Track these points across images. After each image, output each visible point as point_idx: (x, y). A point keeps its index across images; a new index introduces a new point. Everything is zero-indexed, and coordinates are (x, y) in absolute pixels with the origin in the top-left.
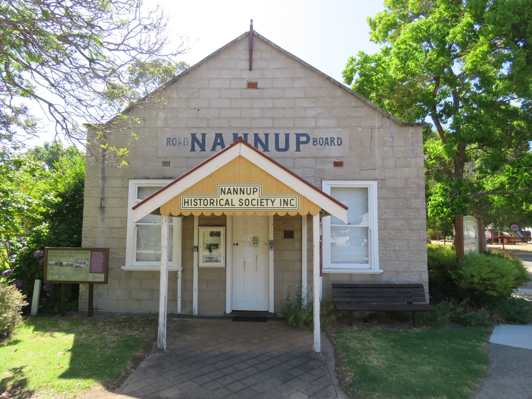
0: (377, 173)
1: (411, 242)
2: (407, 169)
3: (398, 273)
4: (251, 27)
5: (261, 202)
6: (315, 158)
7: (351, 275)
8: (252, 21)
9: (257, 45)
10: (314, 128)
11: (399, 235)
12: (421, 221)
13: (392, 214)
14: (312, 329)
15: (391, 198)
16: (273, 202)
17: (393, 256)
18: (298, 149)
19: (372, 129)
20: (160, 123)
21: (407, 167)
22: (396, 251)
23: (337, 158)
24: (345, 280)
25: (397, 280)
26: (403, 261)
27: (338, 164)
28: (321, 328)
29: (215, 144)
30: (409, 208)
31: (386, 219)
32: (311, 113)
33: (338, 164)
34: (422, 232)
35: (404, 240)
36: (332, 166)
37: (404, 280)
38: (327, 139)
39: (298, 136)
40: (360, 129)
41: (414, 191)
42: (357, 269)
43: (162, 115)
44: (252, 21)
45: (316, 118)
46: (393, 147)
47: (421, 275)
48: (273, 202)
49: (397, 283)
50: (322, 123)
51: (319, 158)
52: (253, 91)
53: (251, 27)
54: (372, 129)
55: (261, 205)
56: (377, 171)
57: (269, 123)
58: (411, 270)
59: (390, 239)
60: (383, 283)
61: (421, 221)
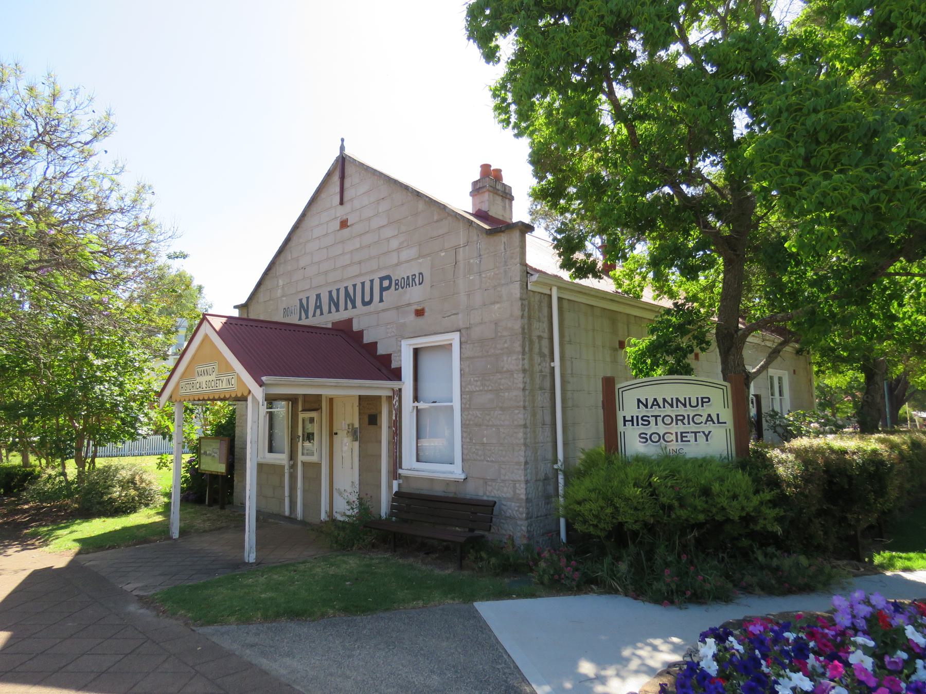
0: (460, 320)
1: (501, 430)
2: (497, 306)
3: (485, 482)
4: (342, 148)
5: (682, 437)
6: (397, 308)
7: (431, 480)
8: (343, 140)
9: (349, 170)
10: (397, 265)
11: (488, 418)
12: (515, 393)
13: (479, 383)
14: (259, 512)
15: (478, 357)
16: (707, 436)
17: (480, 452)
18: (381, 300)
19: (456, 249)
20: (279, 292)
21: (498, 303)
22: (483, 444)
23: (419, 303)
24: (425, 489)
25: (485, 494)
26: (492, 461)
27: (420, 313)
28: (533, 595)
29: (316, 307)
30: (500, 372)
31: (471, 393)
32: (394, 244)
33: (420, 313)
34: (516, 411)
35: (493, 426)
36: (412, 317)
37: (493, 494)
38: (408, 277)
39: (702, 398)
40: (443, 254)
41: (505, 342)
42: (444, 473)
43: (281, 283)
44: (343, 140)
45: (399, 250)
46: (480, 273)
47: (515, 487)
48: (707, 436)
49: (485, 498)
50: (405, 255)
51: (401, 307)
52: (346, 231)
53: (342, 148)
54: (456, 249)
55: (682, 441)
56: (460, 316)
57: (355, 270)
58: (502, 477)
59: (476, 425)
60: (468, 497)
61: (515, 393)
